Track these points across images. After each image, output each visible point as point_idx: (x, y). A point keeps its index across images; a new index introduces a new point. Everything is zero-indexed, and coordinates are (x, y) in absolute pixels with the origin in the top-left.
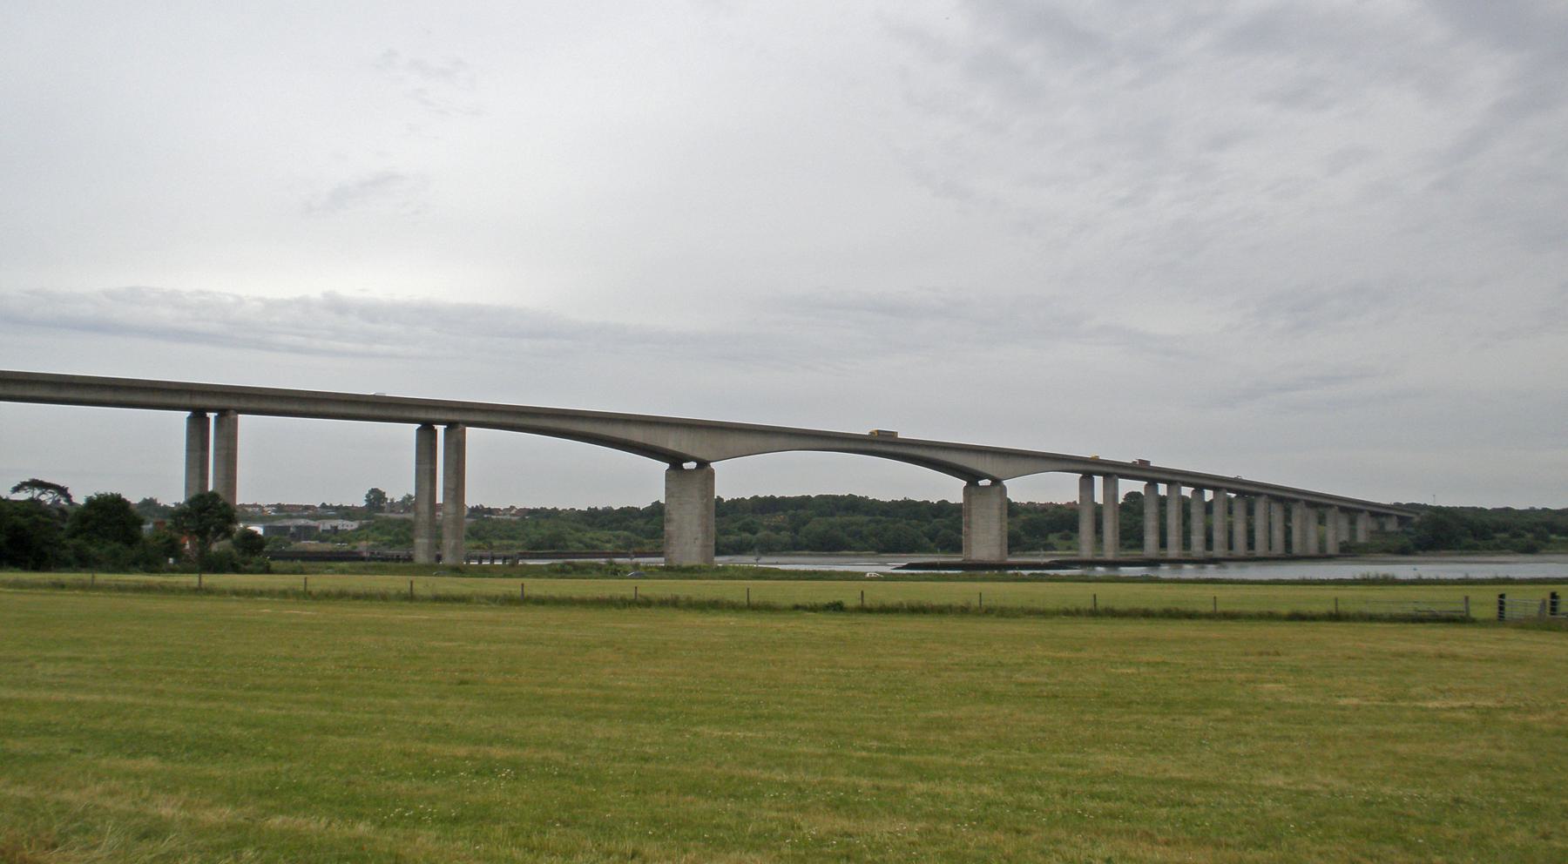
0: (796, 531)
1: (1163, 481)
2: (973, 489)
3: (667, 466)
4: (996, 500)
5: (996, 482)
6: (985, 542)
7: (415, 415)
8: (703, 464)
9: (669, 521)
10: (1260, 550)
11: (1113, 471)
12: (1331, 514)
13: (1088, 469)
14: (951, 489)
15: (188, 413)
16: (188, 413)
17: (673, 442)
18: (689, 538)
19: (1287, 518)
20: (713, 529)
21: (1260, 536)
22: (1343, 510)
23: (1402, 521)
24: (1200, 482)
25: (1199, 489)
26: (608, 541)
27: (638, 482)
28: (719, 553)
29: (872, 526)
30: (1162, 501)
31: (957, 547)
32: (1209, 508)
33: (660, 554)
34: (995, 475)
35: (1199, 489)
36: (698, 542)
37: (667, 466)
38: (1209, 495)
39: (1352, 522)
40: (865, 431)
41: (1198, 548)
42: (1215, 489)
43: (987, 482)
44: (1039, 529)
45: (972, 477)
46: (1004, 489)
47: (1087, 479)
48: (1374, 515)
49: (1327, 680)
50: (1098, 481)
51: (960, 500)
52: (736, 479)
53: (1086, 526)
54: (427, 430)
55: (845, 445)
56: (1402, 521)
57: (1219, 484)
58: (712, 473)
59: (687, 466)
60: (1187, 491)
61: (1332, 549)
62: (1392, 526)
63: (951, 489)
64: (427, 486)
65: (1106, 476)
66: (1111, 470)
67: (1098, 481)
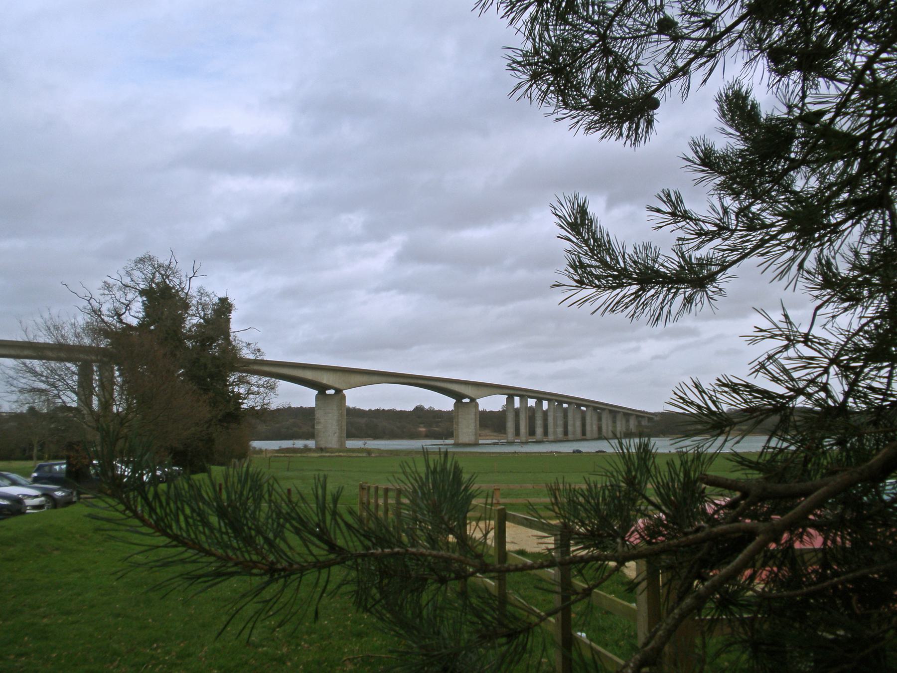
1: (545, 399)
3: (317, 392)
4: (473, 410)
5: (473, 400)
8: (339, 391)
9: (318, 423)
10: (588, 435)
11: (525, 394)
12: (619, 417)
13: (511, 392)
14: (446, 404)
17: (325, 378)
19: (600, 419)
20: (344, 423)
21: (551, 430)
22: (611, 411)
23: (650, 419)
24: (540, 396)
25: (539, 401)
28: (350, 435)
30: (517, 412)
32: (545, 413)
33: (311, 436)
34: (337, 386)
35: (539, 401)
37: (317, 392)
39: (628, 421)
42: (549, 400)
43: (332, 392)
45: (321, 388)
46: (477, 405)
48: (638, 416)
50: (517, 400)
51: (313, 405)
52: (360, 398)
53: (510, 425)
57: (556, 399)
58: (344, 396)
59: (329, 392)
60: (532, 402)
62: (644, 422)
63: (446, 404)
65: (521, 396)
66: (525, 393)
67: (517, 400)
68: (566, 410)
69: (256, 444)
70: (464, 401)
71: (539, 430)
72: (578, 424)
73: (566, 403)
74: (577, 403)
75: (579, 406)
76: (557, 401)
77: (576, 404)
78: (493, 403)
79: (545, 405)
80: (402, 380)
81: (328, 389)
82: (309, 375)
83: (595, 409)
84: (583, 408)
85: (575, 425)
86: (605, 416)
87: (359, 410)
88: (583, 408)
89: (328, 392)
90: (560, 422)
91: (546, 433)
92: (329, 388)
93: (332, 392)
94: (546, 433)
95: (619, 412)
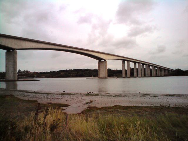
2: (100, 62)
13: (124, 60)
25: (135, 63)
27: (93, 65)
36: (13, 73)
50: (137, 64)
70: (102, 61)
76: (141, 63)
77: (149, 65)
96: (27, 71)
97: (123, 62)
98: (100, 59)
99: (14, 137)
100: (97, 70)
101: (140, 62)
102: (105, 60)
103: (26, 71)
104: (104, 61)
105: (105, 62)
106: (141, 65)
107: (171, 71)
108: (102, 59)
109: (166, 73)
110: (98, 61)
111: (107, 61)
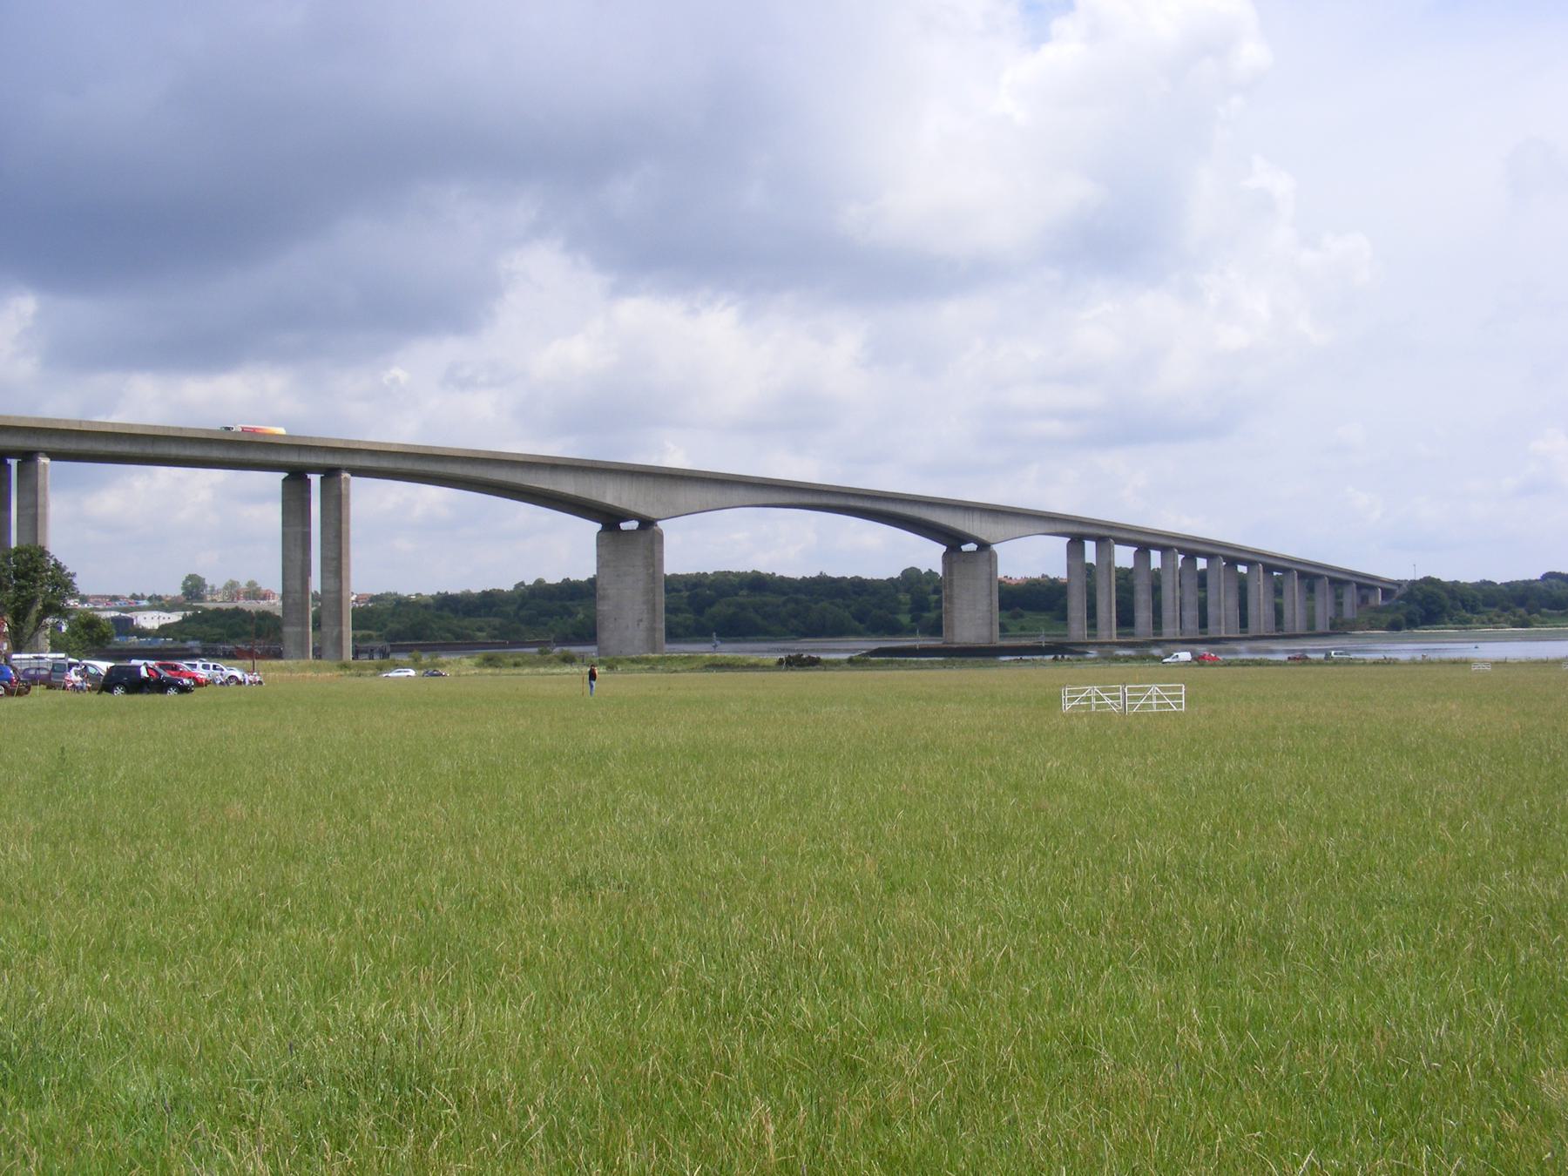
0: (699, 611)
1: (1090, 537)
2: (955, 556)
3: (598, 526)
6: (972, 620)
7: (273, 457)
8: (647, 524)
11: (1106, 534)
12: (1322, 587)
13: (1077, 532)
14: (928, 556)
15: (284, 475)
16: (284, 475)
17: (610, 494)
18: (629, 615)
19: (1278, 592)
21: (1169, 613)
22: (1303, 575)
24: (1144, 543)
25: (1143, 549)
26: (480, 629)
27: (563, 550)
29: (791, 606)
31: (936, 629)
34: (984, 537)
35: (1191, 556)
36: (643, 625)
37: (598, 526)
38: (1202, 564)
40: (1530, 571)
41: (1192, 628)
42: (1164, 549)
44: (1032, 601)
45: (952, 540)
46: (992, 559)
47: (1076, 542)
48: (1360, 586)
49: (632, 1144)
50: (1090, 547)
52: (698, 545)
54: (296, 478)
55: (816, 500)
56: (1387, 593)
57: (1191, 548)
61: (1322, 625)
64: (298, 555)
65: (1100, 540)
66: (1106, 533)
67: (1090, 547)
68: (1202, 576)
69: (14, 545)
70: (965, 548)
71: (1143, 616)
72: (1232, 602)
73: (1243, 562)
74: (1230, 556)
75: (1232, 562)
76: (1181, 551)
77: (1226, 558)
78: (1031, 558)
79: (1156, 558)
80: (816, 500)
81: (626, 519)
82: (567, 485)
83: (1269, 569)
84: (1242, 569)
85: (1260, 608)
86: (1294, 587)
87: (782, 579)
88: (1242, 569)
89: (624, 526)
90: (1191, 599)
91: (1157, 622)
92: (627, 516)
93: (633, 525)
94: (1157, 622)
95: (1319, 577)
96: (251, 584)
97: (1136, 555)
98: (609, 519)
99: (49, 1108)
100: (592, 582)
101: (1173, 543)
102: (984, 546)
103: (243, 585)
104: (640, 527)
105: (985, 554)
106: (1181, 557)
107: (1387, 593)
108: (967, 539)
109: (1324, 608)
110: (944, 548)
111: (995, 547)
